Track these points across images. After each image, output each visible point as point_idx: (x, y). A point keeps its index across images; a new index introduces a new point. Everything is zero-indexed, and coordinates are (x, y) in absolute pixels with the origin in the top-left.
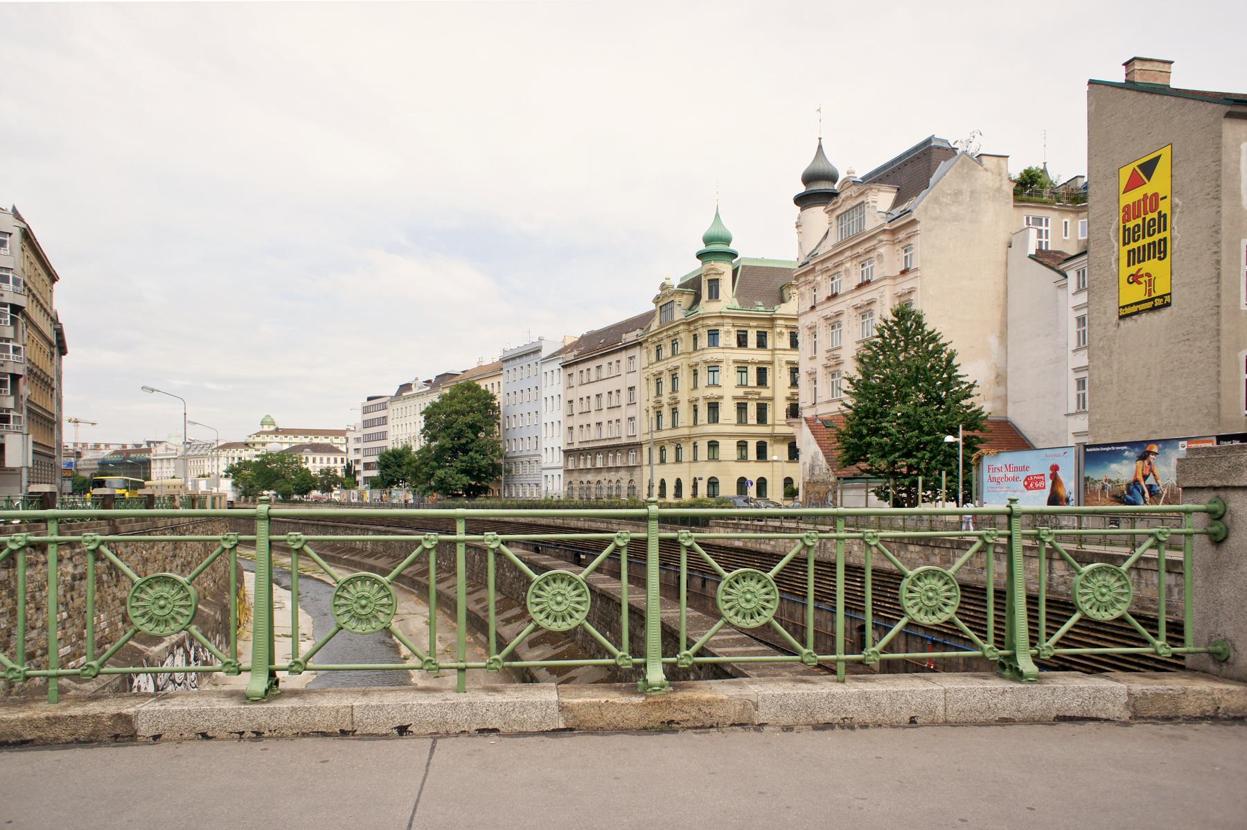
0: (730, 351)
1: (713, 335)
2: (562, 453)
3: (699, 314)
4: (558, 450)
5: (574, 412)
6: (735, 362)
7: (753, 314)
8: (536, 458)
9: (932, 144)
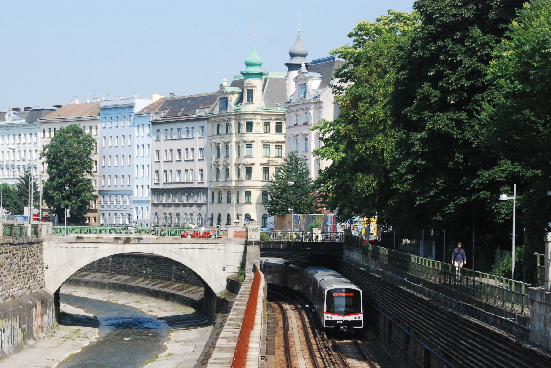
0: (259, 135)
1: (250, 125)
2: (150, 190)
3: (241, 111)
4: (147, 187)
5: (160, 160)
6: (262, 142)
7: (274, 111)
8: (129, 193)
9: (335, 60)
